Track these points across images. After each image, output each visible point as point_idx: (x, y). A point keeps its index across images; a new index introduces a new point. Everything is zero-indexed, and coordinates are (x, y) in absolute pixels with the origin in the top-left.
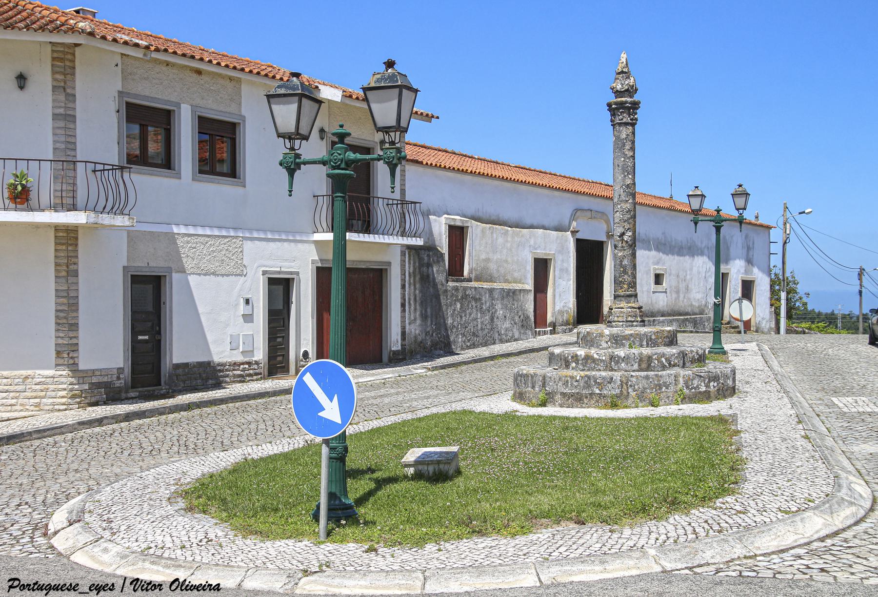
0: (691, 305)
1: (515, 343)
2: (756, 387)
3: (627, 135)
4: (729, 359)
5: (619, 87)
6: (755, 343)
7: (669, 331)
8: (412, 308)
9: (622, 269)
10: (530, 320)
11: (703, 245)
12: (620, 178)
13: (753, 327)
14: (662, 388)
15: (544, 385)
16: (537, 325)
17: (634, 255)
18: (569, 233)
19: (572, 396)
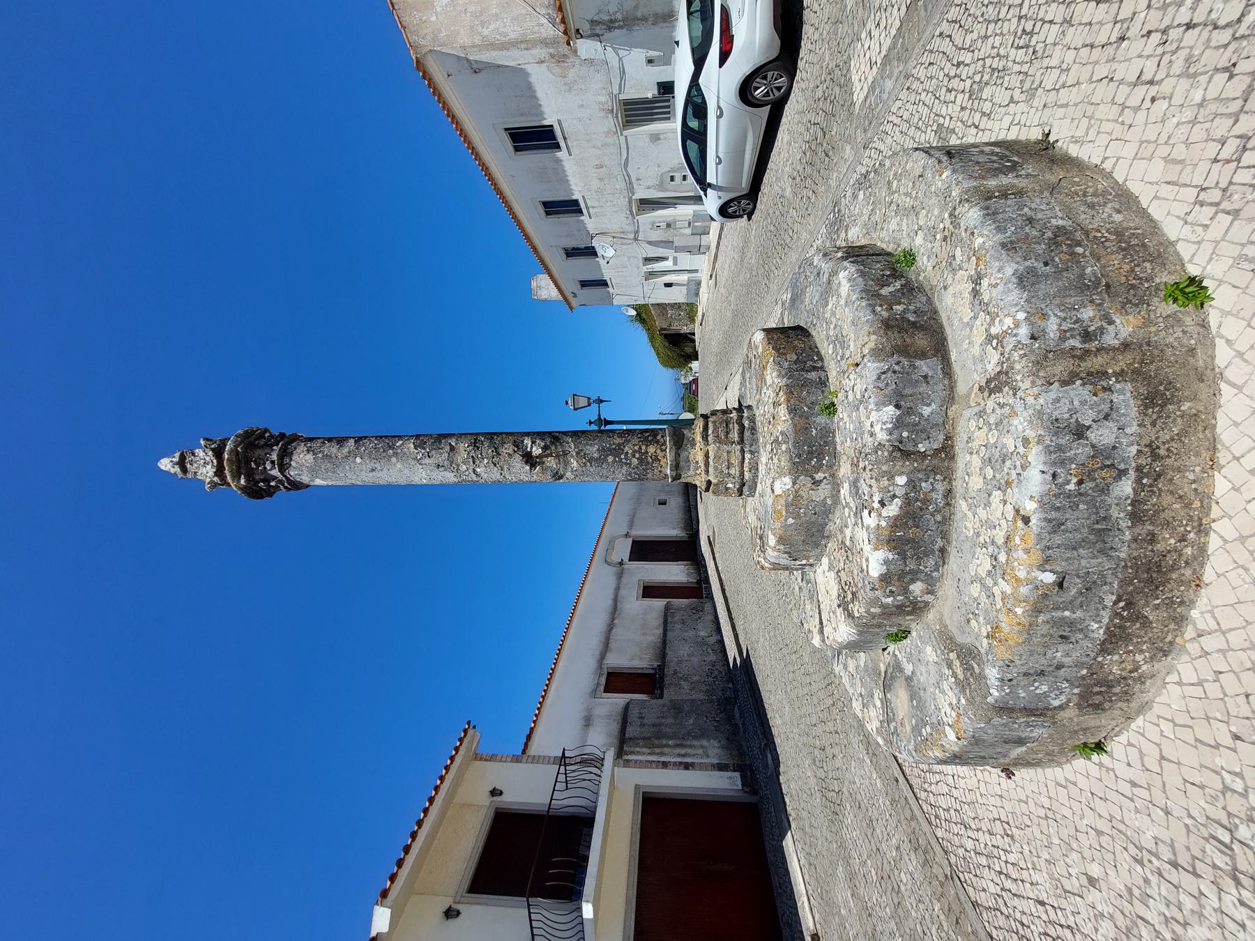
3: (308, 451)
8: (688, 751)
9: (610, 459)
19: (1129, 605)
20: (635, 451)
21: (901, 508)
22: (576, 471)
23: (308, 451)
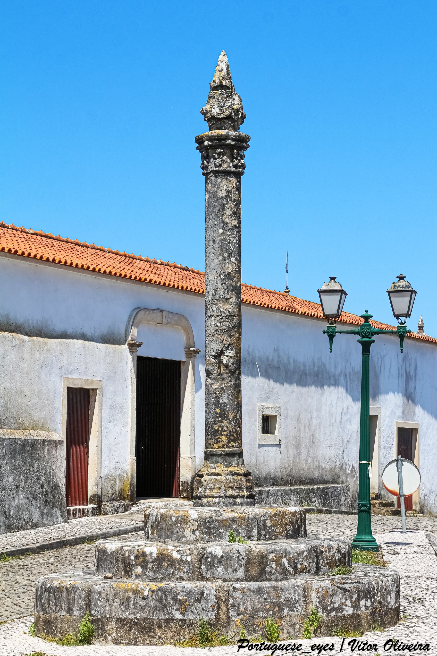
0: (319, 467)
1: (33, 531)
2: (432, 609)
3: (228, 192)
4: (385, 557)
5: (215, 111)
6: (422, 533)
7: (294, 514)
9: (218, 411)
10: (59, 492)
11: (339, 370)
12: (216, 261)
13: (416, 504)
14: (283, 610)
15: (88, 606)
16: (71, 501)
17: (238, 387)
18: (125, 347)
19: (136, 624)
20: (223, 427)
21: (176, 558)
22: (211, 387)
23: (228, 192)
